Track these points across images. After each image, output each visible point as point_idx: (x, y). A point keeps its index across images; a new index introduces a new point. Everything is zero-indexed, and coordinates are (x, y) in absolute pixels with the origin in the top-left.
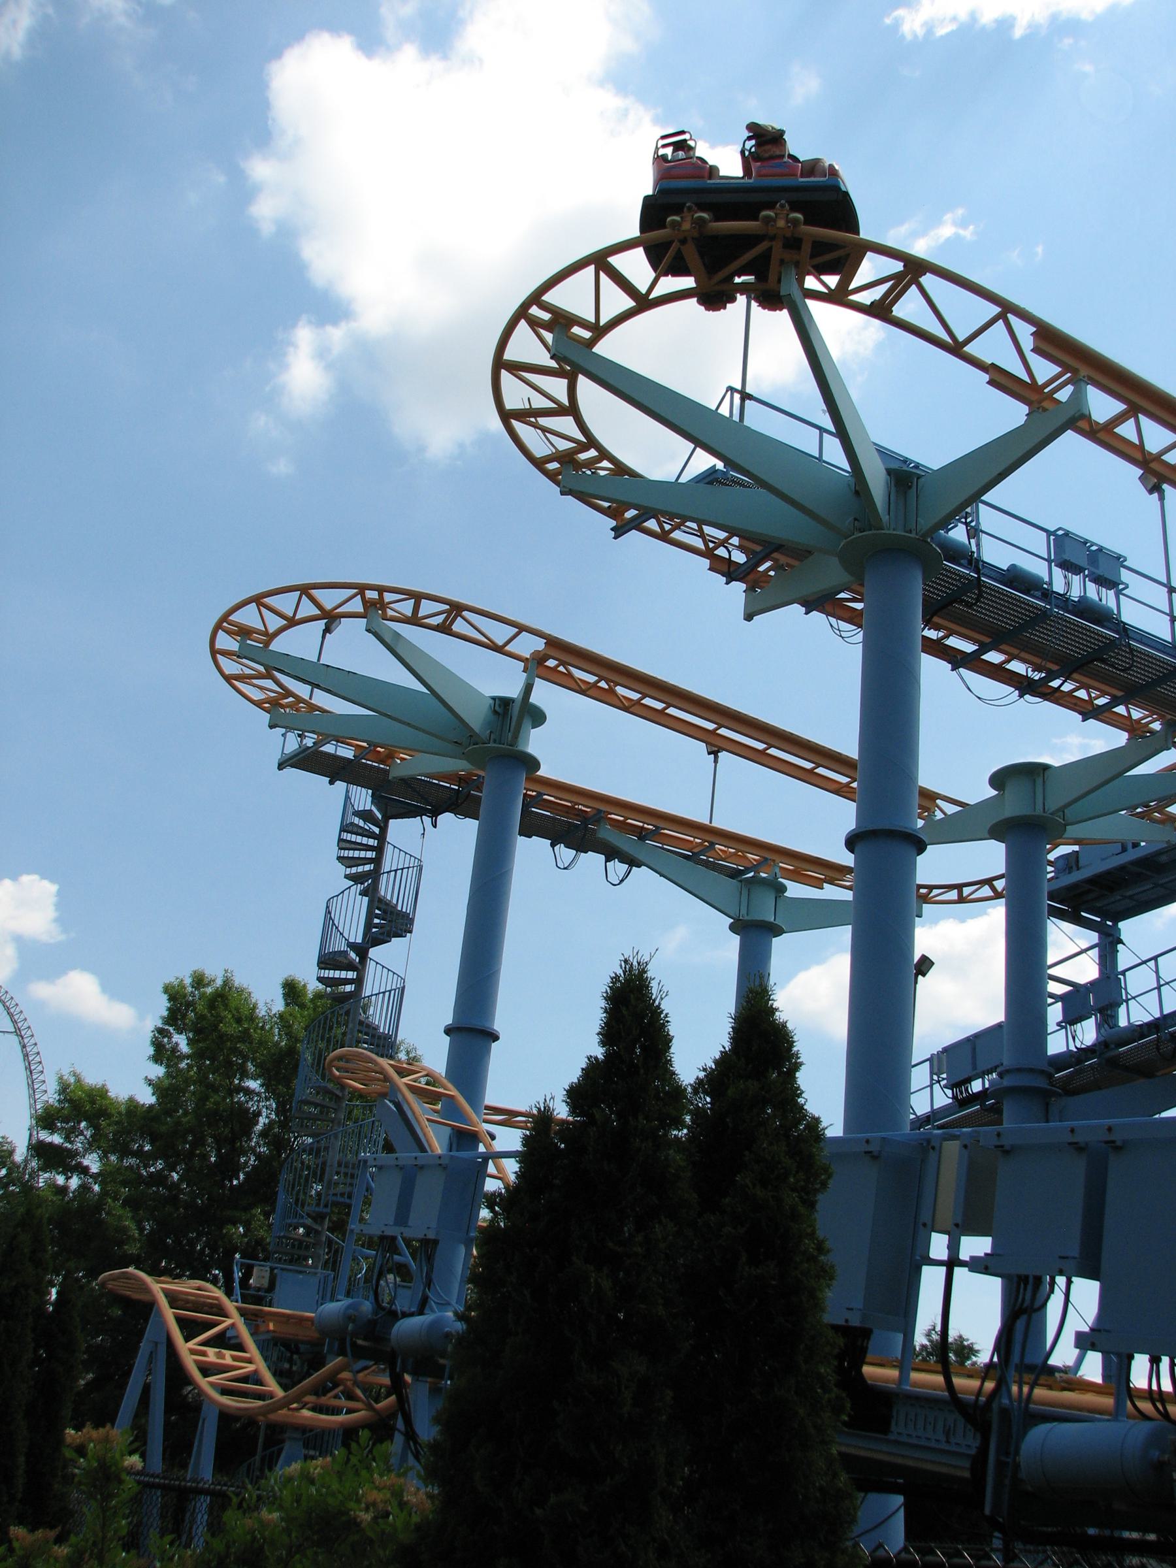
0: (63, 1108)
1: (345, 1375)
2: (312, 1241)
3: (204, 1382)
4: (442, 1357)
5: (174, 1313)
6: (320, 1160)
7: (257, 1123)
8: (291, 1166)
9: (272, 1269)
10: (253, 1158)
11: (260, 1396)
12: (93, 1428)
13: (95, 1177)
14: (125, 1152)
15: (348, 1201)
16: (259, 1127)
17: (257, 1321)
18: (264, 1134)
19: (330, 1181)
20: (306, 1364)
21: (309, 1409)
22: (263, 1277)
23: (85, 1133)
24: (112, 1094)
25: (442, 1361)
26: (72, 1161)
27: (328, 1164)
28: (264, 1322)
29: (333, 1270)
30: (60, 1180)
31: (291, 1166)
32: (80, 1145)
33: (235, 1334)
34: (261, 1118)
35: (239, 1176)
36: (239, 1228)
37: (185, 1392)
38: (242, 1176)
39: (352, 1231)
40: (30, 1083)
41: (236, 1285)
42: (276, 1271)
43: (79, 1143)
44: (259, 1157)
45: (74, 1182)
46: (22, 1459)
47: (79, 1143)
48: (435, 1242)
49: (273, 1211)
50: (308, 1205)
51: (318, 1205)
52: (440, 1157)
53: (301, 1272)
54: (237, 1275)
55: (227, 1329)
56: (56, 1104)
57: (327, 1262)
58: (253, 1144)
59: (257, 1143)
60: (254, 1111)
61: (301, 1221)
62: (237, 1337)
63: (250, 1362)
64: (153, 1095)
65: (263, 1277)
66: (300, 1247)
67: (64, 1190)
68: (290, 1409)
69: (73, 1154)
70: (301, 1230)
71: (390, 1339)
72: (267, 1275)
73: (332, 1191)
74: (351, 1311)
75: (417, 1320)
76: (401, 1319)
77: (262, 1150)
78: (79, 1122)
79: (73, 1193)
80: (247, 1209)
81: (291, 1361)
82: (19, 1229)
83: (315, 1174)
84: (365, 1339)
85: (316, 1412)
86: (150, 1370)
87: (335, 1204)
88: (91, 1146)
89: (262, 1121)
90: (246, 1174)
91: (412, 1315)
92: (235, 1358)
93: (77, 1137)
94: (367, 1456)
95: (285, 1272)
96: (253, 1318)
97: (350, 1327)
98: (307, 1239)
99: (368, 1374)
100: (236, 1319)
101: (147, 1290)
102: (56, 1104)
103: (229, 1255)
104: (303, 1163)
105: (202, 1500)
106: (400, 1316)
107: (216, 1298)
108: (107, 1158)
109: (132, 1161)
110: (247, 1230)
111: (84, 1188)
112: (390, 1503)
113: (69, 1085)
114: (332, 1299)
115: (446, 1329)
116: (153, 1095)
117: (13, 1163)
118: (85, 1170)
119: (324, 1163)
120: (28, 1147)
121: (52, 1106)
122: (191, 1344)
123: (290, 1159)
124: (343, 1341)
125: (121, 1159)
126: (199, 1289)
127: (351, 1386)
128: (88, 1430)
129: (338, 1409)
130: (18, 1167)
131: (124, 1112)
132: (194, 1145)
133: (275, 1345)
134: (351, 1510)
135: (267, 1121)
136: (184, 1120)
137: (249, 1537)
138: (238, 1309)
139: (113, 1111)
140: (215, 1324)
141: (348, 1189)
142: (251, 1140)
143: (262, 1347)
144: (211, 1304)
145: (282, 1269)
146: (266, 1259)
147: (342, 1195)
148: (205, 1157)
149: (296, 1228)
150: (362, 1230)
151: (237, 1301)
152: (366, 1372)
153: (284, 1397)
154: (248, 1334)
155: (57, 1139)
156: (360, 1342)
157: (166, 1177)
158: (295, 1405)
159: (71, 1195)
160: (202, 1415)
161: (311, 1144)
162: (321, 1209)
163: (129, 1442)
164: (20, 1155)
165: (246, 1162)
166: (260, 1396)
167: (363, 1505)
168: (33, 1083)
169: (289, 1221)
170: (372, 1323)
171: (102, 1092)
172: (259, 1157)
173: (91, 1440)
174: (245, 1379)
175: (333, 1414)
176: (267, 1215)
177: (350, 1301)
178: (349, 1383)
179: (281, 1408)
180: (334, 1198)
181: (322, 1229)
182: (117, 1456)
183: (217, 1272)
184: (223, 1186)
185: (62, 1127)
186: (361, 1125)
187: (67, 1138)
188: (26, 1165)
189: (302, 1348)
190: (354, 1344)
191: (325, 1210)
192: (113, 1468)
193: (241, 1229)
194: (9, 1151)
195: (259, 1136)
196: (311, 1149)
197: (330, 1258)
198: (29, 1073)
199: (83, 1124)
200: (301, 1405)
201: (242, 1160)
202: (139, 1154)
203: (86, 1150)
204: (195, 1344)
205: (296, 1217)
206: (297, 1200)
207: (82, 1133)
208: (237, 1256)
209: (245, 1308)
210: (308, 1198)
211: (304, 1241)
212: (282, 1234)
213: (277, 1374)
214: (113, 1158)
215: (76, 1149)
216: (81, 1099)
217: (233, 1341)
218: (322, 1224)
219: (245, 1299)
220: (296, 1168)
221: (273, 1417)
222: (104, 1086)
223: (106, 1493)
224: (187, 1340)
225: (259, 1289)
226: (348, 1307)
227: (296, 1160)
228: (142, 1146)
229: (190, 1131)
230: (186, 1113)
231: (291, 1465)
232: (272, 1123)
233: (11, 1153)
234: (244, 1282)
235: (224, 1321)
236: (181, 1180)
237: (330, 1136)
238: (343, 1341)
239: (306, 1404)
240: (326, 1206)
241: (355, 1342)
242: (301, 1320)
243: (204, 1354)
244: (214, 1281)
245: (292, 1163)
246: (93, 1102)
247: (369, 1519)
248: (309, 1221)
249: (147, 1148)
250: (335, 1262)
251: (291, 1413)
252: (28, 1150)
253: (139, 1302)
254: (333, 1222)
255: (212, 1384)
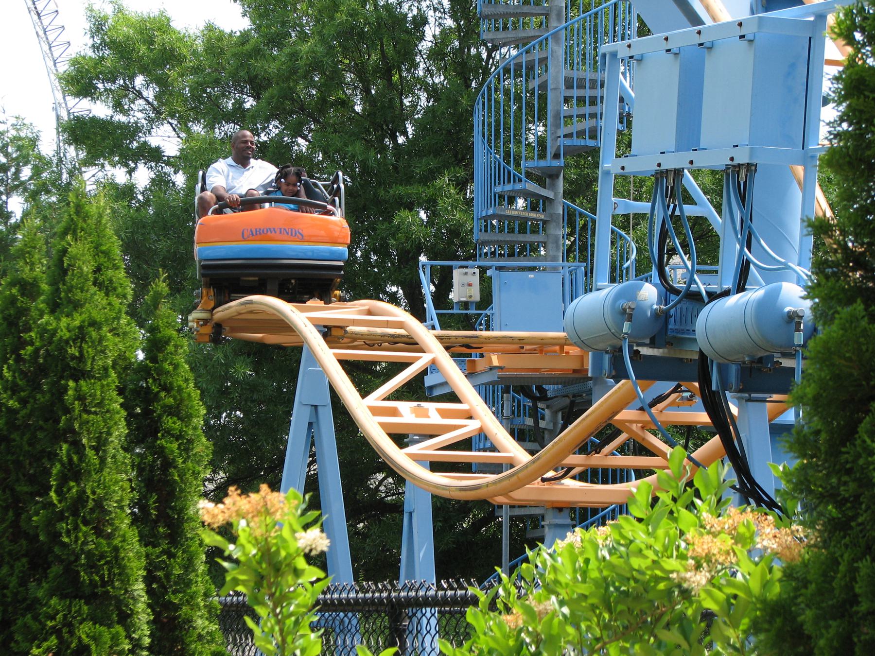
0: (102, 58)
1: (625, 415)
2: (542, 217)
3: (398, 456)
4: (786, 355)
5: (335, 354)
6: (534, 84)
7: (422, 38)
8: (489, 100)
9: (483, 270)
10: (423, 96)
11: (495, 468)
12: (240, 495)
13: (173, 163)
14: (217, 116)
15: (591, 143)
16: (425, 45)
17: (470, 355)
18: (436, 54)
19: (557, 115)
20: (560, 415)
21: (574, 478)
22: (470, 285)
23: (145, 94)
24: (177, 25)
25: (786, 363)
26: (131, 142)
27: (550, 87)
28: (482, 356)
29: (583, 259)
30: (120, 176)
31: (489, 100)
32: (140, 115)
33: (442, 380)
34: (427, 28)
35: (406, 128)
36: (418, 212)
37: (372, 484)
38: (410, 130)
39: (607, 173)
40: (41, 33)
41: (429, 304)
42: (489, 273)
43: (138, 113)
44: (433, 92)
45: (143, 176)
46: (139, 588)
47: (138, 113)
48: (751, 168)
49: (470, 178)
50: (526, 159)
51: (542, 156)
52: (740, 25)
53: (532, 269)
54: (428, 289)
55: (424, 372)
56: (90, 53)
57: (570, 250)
58: (421, 73)
59: (428, 70)
60: (414, 17)
61: (519, 186)
62: (445, 384)
63: (471, 418)
64: (244, 15)
65: (470, 285)
66: (523, 230)
67: (128, 192)
68: (544, 480)
69: (132, 131)
70: (521, 203)
71: (695, 340)
72: (476, 280)
73: (563, 131)
74: (623, 303)
75: (733, 300)
76: (709, 302)
77: (437, 81)
78: (132, 78)
79: (143, 193)
80: (429, 177)
81: (535, 414)
82: (69, 237)
83: (530, 106)
84: (653, 344)
85: (586, 481)
86: (313, 455)
87: (570, 151)
88: (157, 115)
89: (431, 31)
90: (417, 124)
91: (726, 293)
92: (444, 414)
93: (133, 101)
94: (685, 490)
95: (505, 274)
96: (464, 350)
97: (626, 327)
98: (533, 215)
99: (664, 409)
100: (436, 352)
101: (284, 326)
102: (90, 53)
103: (409, 259)
104: (507, 92)
105: (428, 615)
106: (706, 300)
107: (400, 325)
108: (188, 130)
109: (229, 128)
110: (433, 215)
111: (160, 182)
112: (735, 553)
113: (106, 19)
114: (588, 289)
115: (787, 309)
116: (244, 15)
117: (40, 157)
118: (154, 155)
119: (543, 86)
120: (57, 129)
121: (84, 57)
122: (375, 398)
123: (485, 87)
124: (616, 355)
125: (211, 127)
126: (370, 313)
127: (640, 432)
128: (234, 500)
129: (622, 470)
130: (50, 163)
131: (200, 49)
132: (326, 88)
133: (506, 390)
134: (672, 572)
135: (438, 31)
136: (305, 48)
137: (511, 643)
138: (440, 338)
139: (184, 51)
140: (403, 366)
141: (587, 124)
142: (416, 66)
143: (489, 394)
144: (393, 336)
145: (500, 268)
146: (472, 257)
147: (581, 134)
148: (345, 104)
149: (512, 200)
150: (623, 168)
151: (433, 328)
152: (660, 406)
153: (533, 462)
154: (463, 376)
155: (101, 110)
156: (645, 351)
157: (289, 147)
158: (551, 474)
159: (140, 197)
160: (406, 508)
161: (516, 57)
162: (549, 162)
163: (299, 512)
164: (48, 146)
165: (414, 106)
166: (495, 468)
167: (691, 562)
168: (45, 32)
169: (499, 189)
170: (662, 318)
171: (163, 25)
172: (433, 92)
173: (240, 515)
174: (465, 444)
175: (614, 482)
176: (462, 184)
177: (617, 287)
178: (634, 427)
179: (530, 479)
180: (568, 142)
181: (556, 195)
182: (286, 533)
183: (394, 289)
184: (383, 149)
185: (106, 90)
186: (596, 14)
187: (118, 106)
188: (60, 160)
189: (550, 389)
190: (635, 355)
191: (556, 163)
192: (283, 554)
193: (423, 215)
194: (31, 140)
195: (429, 57)
196: (518, 66)
197: (573, 243)
198: (36, 17)
199: (139, 80)
200: (561, 473)
201: (407, 102)
202: (239, 115)
203: (151, 121)
204: (377, 399)
205: (509, 181)
206: (507, 155)
207: (139, 95)
208: (423, 259)
209: (449, 337)
210: (523, 149)
211: (527, 219)
212: (491, 212)
213: (519, 435)
214: (197, 128)
215: (136, 123)
216: (128, 38)
217: (437, 392)
218: (553, 187)
219: (446, 322)
220: (497, 102)
221: (520, 495)
222: (162, 13)
223: (277, 594)
224: (364, 394)
225: (466, 305)
226: (618, 296)
227: (496, 90)
228: (240, 103)
229: (316, 65)
230: (303, 37)
231: (566, 537)
232: (445, 33)
233: (34, 142)
234: (441, 298)
235: (419, 358)
236: (312, 145)
237: (547, 39)
238: (616, 355)
239: (570, 469)
240: (556, 156)
241: (638, 352)
242: (542, 347)
243: (394, 412)
244: (393, 299)
245: (490, 96)
246: (150, 41)
247: (704, 581)
248: (532, 186)
249: (249, 103)
250: (583, 248)
251: (546, 485)
252: (58, 133)
253: (279, 347)
254: (571, 183)
255: (410, 456)
